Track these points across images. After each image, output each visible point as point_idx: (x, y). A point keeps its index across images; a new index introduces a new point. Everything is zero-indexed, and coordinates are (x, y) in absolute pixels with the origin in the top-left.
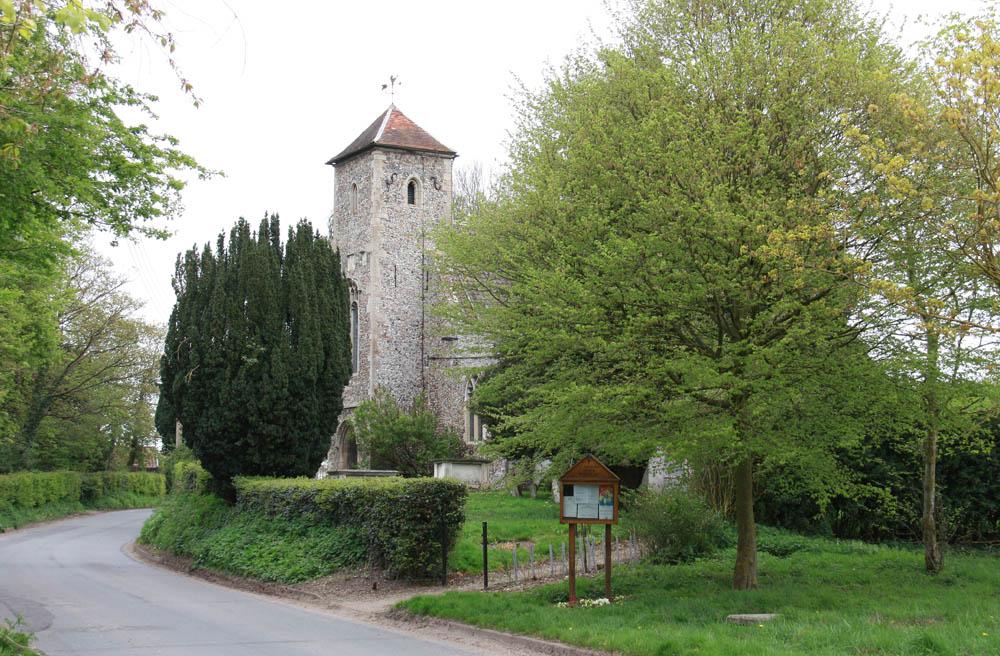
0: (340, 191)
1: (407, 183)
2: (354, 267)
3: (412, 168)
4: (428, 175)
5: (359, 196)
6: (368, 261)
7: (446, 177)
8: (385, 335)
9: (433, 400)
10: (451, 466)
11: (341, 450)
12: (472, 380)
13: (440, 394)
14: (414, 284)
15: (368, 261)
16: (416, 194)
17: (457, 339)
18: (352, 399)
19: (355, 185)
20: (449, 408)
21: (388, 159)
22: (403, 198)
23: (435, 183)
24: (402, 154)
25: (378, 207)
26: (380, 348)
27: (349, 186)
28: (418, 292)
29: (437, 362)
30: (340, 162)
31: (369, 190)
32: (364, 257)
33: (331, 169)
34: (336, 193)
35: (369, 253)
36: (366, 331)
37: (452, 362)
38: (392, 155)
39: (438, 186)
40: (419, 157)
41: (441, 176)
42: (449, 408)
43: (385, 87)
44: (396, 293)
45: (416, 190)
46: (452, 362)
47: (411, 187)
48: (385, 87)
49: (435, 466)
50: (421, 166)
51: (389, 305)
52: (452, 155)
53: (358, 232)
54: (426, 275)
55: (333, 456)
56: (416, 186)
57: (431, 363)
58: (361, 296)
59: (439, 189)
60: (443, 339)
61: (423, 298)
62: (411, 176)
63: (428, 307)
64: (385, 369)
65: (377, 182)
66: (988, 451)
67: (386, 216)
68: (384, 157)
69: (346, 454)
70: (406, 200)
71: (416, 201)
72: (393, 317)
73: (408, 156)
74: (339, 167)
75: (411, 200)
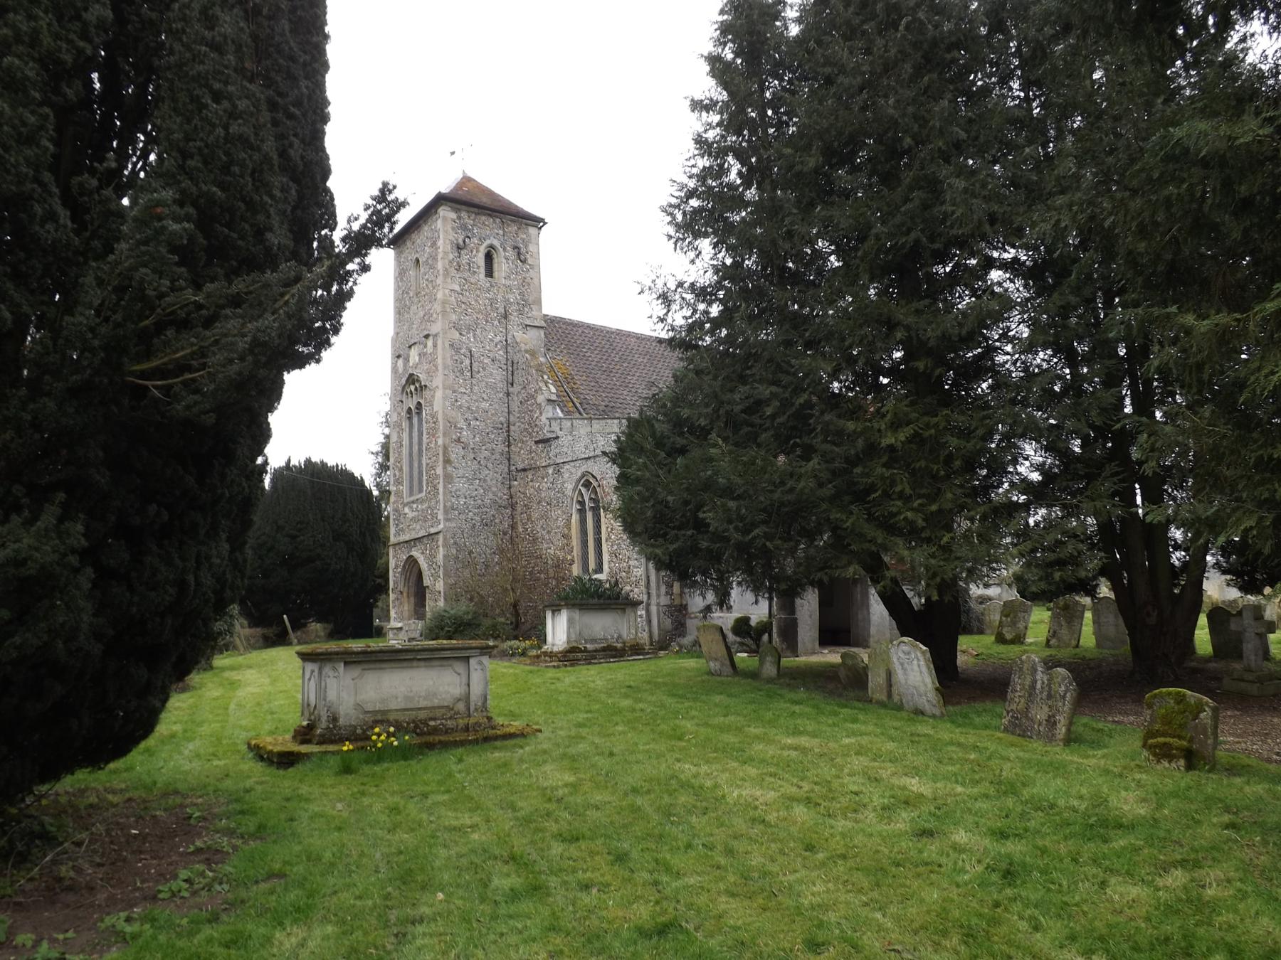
1: (483, 250)
2: (417, 358)
3: (490, 233)
4: (510, 242)
5: (422, 270)
6: (435, 346)
7: (531, 248)
8: (458, 440)
10: (576, 614)
11: (405, 594)
12: (583, 490)
13: (535, 515)
14: (497, 376)
15: (435, 346)
16: (496, 266)
17: (557, 438)
18: (418, 527)
19: (418, 261)
20: (549, 532)
21: (459, 218)
22: (478, 267)
23: (519, 254)
26: (453, 457)
27: (411, 264)
28: (502, 386)
31: (435, 259)
32: (430, 343)
34: (396, 278)
35: (436, 335)
36: (434, 436)
37: (550, 471)
38: (464, 214)
39: (522, 258)
40: (498, 220)
41: (526, 246)
42: (549, 532)
43: (453, 153)
45: (496, 260)
46: (550, 471)
47: (489, 258)
48: (453, 153)
49: (549, 615)
50: (501, 232)
51: (463, 401)
52: (537, 222)
53: (422, 314)
54: (511, 367)
55: (397, 603)
56: (495, 256)
57: (521, 475)
58: (426, 393)
59: (524, 262)
60: (536, 442)
61: (508, 394)
62: (488, 242)
63: (515, 406)
64: (460, 485)
67: (457, 288)
68: (453, 215)
69: (412, 599)
70: (483, 270)
71: (496, 274)
73: (483, 218)
74: (399, 247)
75: (489, 273)
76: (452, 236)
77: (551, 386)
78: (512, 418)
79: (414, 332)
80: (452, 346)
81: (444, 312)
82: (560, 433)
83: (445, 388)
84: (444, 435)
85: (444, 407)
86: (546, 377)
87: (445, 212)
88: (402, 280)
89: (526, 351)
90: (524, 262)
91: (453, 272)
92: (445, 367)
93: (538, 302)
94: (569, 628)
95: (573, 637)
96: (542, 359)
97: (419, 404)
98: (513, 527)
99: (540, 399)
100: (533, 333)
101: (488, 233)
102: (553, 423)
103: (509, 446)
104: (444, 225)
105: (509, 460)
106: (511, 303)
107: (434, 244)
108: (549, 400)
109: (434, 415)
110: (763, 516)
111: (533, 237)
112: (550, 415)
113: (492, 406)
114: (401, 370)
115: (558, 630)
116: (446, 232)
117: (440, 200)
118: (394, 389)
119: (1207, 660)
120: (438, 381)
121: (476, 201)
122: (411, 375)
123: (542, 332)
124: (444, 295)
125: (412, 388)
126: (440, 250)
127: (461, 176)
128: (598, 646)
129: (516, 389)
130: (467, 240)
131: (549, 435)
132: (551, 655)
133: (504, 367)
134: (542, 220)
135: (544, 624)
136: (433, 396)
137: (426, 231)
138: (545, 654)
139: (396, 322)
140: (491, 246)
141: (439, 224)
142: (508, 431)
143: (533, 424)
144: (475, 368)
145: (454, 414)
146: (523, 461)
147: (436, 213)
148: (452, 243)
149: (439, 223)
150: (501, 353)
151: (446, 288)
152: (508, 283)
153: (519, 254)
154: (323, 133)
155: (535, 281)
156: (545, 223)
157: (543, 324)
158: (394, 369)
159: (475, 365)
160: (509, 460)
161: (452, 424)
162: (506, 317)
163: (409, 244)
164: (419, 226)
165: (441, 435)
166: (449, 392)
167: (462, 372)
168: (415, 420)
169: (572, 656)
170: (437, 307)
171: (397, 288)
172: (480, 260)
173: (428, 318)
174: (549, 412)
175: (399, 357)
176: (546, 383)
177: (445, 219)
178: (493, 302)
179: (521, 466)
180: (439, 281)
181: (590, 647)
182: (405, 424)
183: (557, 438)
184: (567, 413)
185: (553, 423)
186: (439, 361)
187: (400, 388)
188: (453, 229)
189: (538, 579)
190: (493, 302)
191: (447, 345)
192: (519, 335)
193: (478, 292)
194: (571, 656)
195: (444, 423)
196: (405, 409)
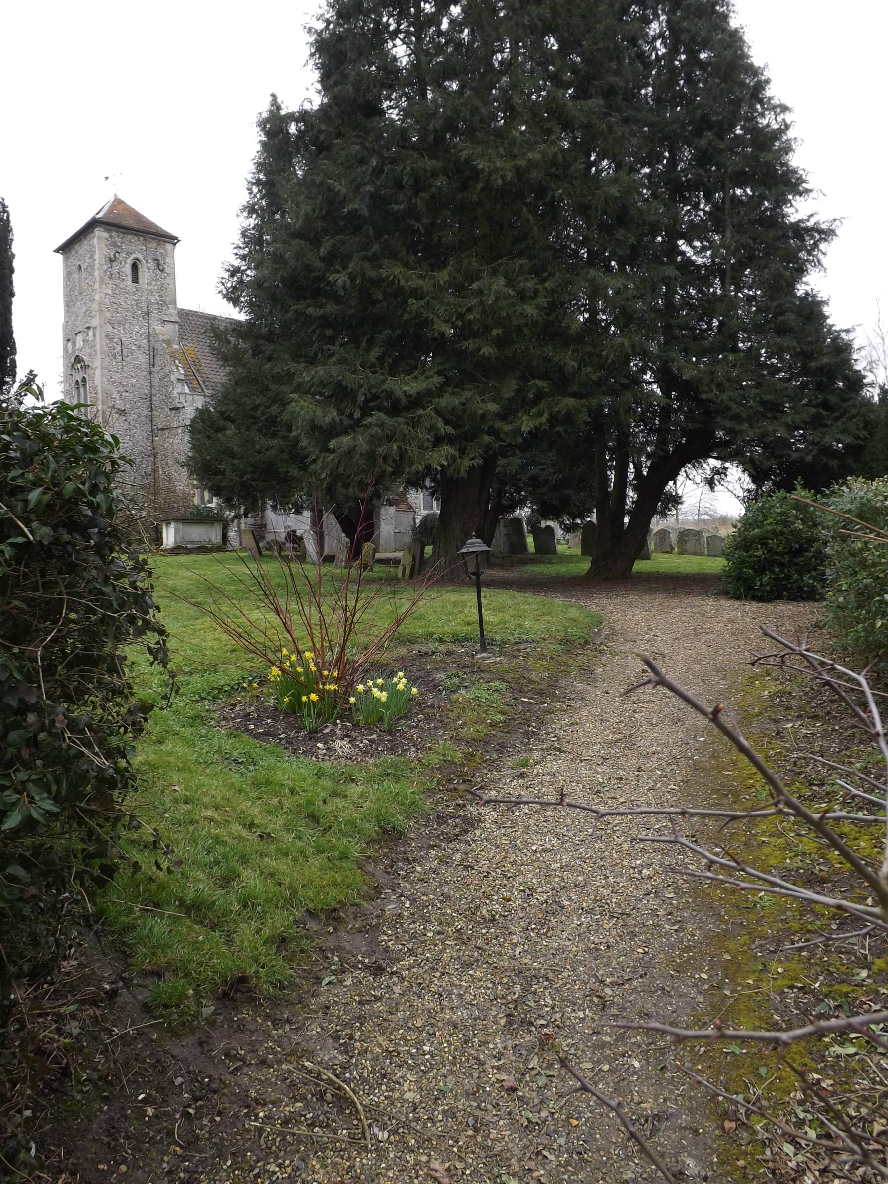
0: (68, 275)
1: (130, 261)
2: (82, 344)
3: (136, 249)
4: (151, 256)
6: (94, 336)
7: (168, 260)
9: (163, 468)
10: (180, 526)
14: (142, 359)
15: (94, 336)
16: (140, 274)
17: (184, 407)
19: (80, 267)
21: (111, 237)
22: (126, 276)
23: (158, 265)
24: (126, 233)
25: (101, 282)
27: (75, 269)
28: (146, 366)
29: (166, 432)
30: (65, 248)
31: (92, 267)
32: (91, 333)
33: (59, 257)
34: (64, 278)
38: (114, 234)
39: (161, 268)
40: (141, 238)
41: (164, 258)
42: (179, 474)
43: (107, 178)
44: (123, 366)
45: (140, 270)
47: (135, 267)
48: (107, 178)
50: (144, 248)
51: (116, 377)
52: (173, 240)
53: (84, 309)
54: (153, 353)
56: (139, 266)
59: (162, 271)
60: (171, 410)
61: (151, 373)
62: (134, 256)
63: (156, 382)
65: (99, 258)
66: (523, 512)
67: (110, 292)
68: (106, 235)
70: (130, 278)
71: (140, 281)
72: (121, 389)
73: (130, 237)
75: (135, 280)
76: (105, 251)
77: (181, 369)
78: (154, 391)
79: (78, 322)
80: (107, 336)
81: (100, 311)
82: (185, 404)
83: (102, 368)
84: (103, 403)
85: (102, 383)
86: (177, 362)
87: (99, 233)
88: (68, 280)
89: (163, 341)
90: (162, 271)
91: (107, 280)
92: (102, 353)
93: (174, 302)
94: (175, 534)
95: (178, 540)
96: (176, 347)
97: (84, 378)
98: (155, 471)
99: (173, 378)
100: (169, 327)
101: (134, 248)
102: (181, 397)
103: (151, 411)
104: (99, 243)
105: (152, 421)
106: (152, 304)
107: (92, 257)
108: (178, 379)
109: (95, 388)
110: (249, 469)
111: (169, 251)
112: (180, 390)
113: (138, 382)
114: (70, 351)
115: (169, 536)
116: (100, 248)
117: (93, 224)
118: (65, 369)
119: (532, 554)
120: (97, 363)
121: (124, 223)
122: (78, 356)
123: (177, 326)
124: (101, 298)
125: (79, 365)
126: (96, 262)
127: (112, 199)
128: (195, 546)
129: (156, 369)
130: (117, 255)
131: (179, 405)
132: (164, 550)
133: (147, 352)
134: (176, 238)
135: (161, 533)
136: (94, 374)
137: (85, 244)
138: (162, 550)
139: (65, 313)
140: (136, 259)
141: (95, 241)
142: (151, 400)
143: (168, 396)
144: (125, 354)
145: (109, 387)
146: (162, 423)
147: (93, 232)
148: (105, 256)
149: (95, 240)
150: (145, 341)
151: (100, 293)
152: (150, 287)
153: (158, 265)
154: (11, 303)
155: (171, 286)
156: (178, 241)
157: (177, 319)
158: (65, 350)
159: (124, 351)
160: (152, 421)
161: (108, 395)
162: (148, 314)
163: (73, 252)
164: (81, 240)
165: (100, 403)
166: (105, 371)
167: (115, 356)
168: (82, 390)
169: (177, 550)
170: (95, 307)
171: (66, 286)
172: (128, 269)
173: (88, 314)
174: (178, 388)
175: (68, 340)
176: (177, 366)
177: (99, 238)
178: (138, 303)
179: (160, 426)
180: (97, 286)
181: (189, 546)
182: (74, 393)
183: (184, 407)
184: (193, 389)
185: (181, 397)
186: (98, 347)
187: (70, 365)
188: (106, 245)
189: (173, 507)
190: (138, 303)
191: (103, 335)
192: (158, 328)
193: (126, 295)
194: (176, 550)
195: (102, 396)
196: (74, 381)
